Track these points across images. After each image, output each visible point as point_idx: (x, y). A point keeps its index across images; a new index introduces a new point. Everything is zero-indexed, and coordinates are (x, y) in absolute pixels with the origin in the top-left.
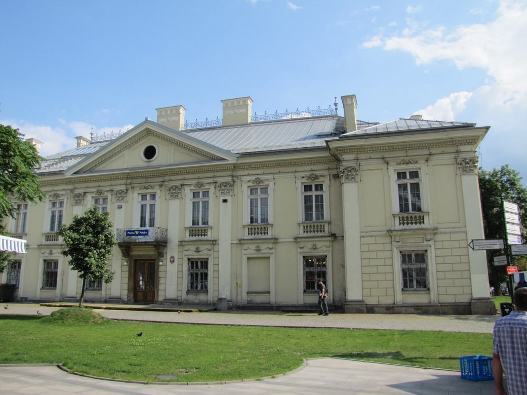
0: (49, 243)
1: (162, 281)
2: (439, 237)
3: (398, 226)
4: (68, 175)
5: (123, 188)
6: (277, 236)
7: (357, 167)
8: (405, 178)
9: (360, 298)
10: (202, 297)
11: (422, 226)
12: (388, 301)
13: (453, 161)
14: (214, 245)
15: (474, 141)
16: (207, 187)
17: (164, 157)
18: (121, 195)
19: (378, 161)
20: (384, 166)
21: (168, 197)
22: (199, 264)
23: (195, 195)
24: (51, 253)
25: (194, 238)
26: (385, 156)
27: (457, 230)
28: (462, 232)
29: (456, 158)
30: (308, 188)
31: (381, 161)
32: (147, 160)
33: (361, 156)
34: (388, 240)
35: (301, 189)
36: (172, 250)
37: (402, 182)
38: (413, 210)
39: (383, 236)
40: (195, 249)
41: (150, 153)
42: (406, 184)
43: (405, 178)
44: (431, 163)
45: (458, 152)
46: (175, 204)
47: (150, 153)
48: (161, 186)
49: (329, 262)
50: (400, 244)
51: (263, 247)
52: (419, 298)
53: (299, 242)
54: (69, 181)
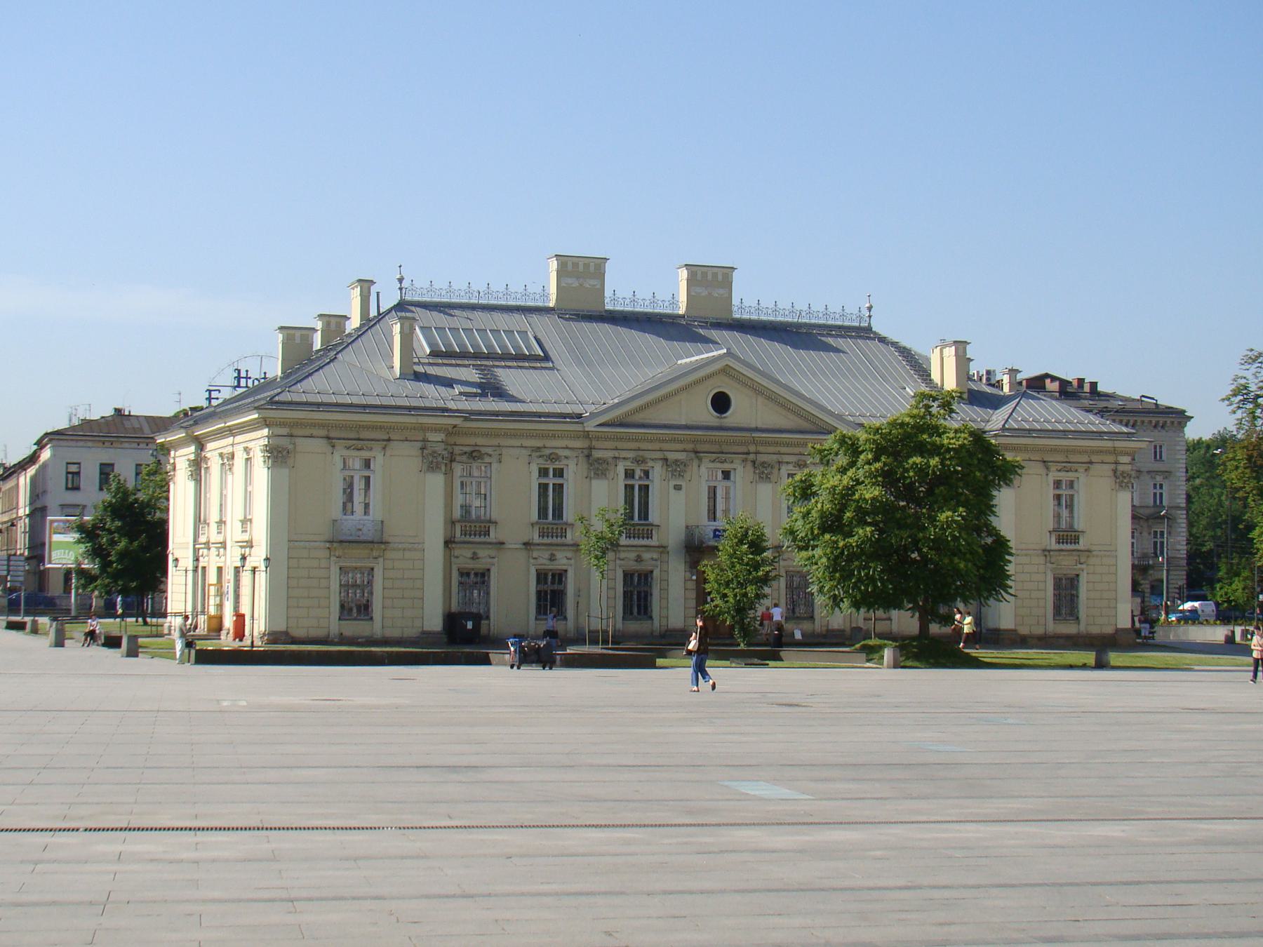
2: (1092, 561)
3: (1054, 546)
4: (590, 426)
5: (681, 456)
6: (501, 540)
9: (1011, 626)
12: (1039, 631)
13: (1111, 473)
16: (651, 464)
17: (743, 410)
18: (676, 468)
20: (1042, 470)
21: (425, 467)
23: (629, 474)
24: (552, 558)
25: (546, 540)
29: (1115, 471)
30: (543, 472)
34: (1042, 559)
35: (535, 473)
41: (721, 403)
46: (765, 490)
47: (721, 403)
52: (1069, 629)
54: (587, 435)
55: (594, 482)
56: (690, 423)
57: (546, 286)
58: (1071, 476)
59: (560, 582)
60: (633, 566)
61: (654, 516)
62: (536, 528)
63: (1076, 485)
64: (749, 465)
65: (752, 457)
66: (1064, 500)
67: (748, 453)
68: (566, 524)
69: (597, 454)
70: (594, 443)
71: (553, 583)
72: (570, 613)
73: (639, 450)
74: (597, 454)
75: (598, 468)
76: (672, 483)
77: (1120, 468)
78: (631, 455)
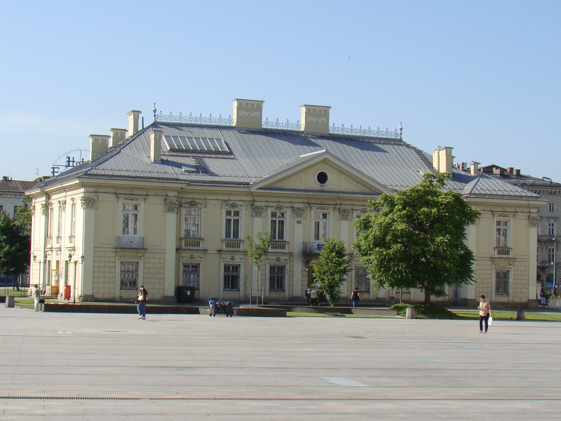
0: (229, 249)
2: (516, 264)
4: (253, 189)
5: (301, 206)
7: (96, 198)
11: (508, 256)
13: (527, 218)
14: (290, 256)
16: (285, 209)
21: (166, 210)
23: (274, 215)
24: (233, 258)
25: (229, 249)
29: (529, 217)
30: (228, 213)
31: (490, 213)
34: (490, 263)
35: (224, 214)
40: (230, 258)
41: (322, 178)
44: (517, 217)
46: (345, 224)
47: (322, 178)
49: (242, 267)
51: (236, 257)
54: (251, 194)
55: (256, 219)
58: (506, 219)
59: (237, 271)
60: (275, 263)
64: (337, 210)
65: (338, 206)
68: (285, 242)
70: (256, 198)
71: (233, 271)
72: (286, 288)
74: (257, 204)
75: (257, 211)
76: (296, 220)
78: (275, 204)
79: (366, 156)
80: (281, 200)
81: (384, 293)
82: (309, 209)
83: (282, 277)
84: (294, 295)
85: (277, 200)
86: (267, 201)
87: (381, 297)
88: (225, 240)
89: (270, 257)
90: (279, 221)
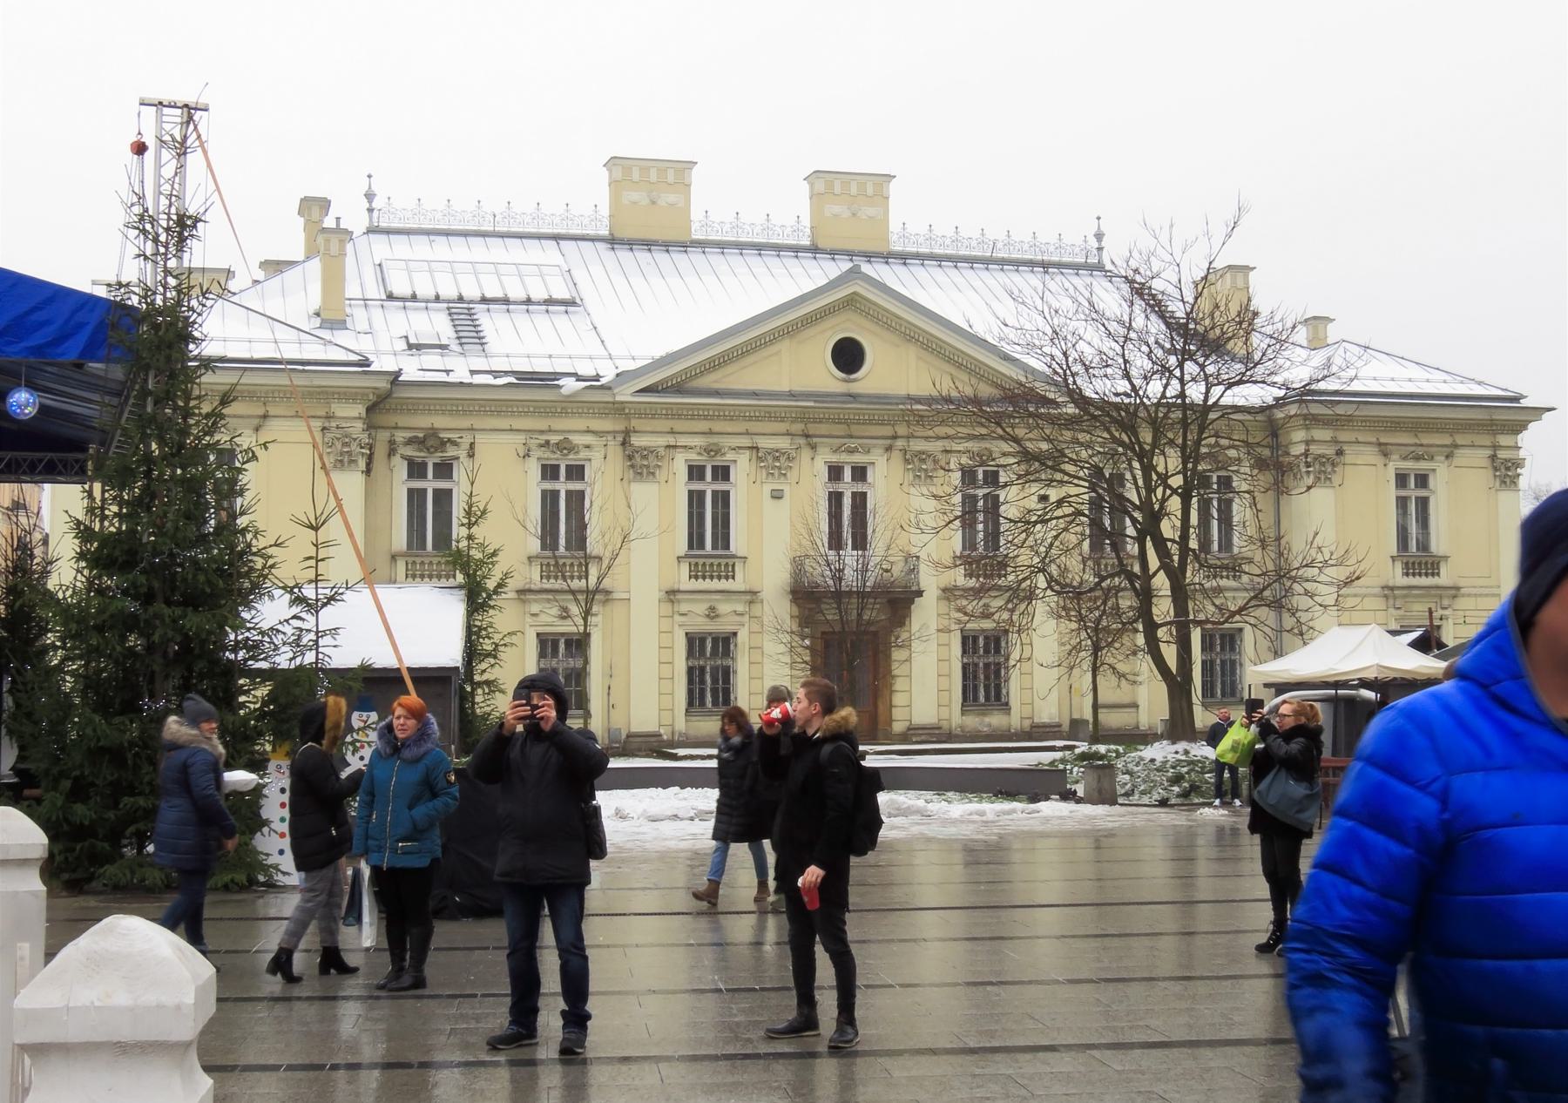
0: (547, 585)
1: (899, 684)
2: (1462, 603)
4: (625, 394)
5: (783, 443)
8: (702, 478)
10: (996, 720)
13: (1486, 463)
15: (1518, 427)
17: (891, 371)
19: (1369, 448)
20: (1379, 460)
22: (562, 646)
23: (695, 472)
26: (1341, 438)
27: (1486, 591)
28: (1493, 595)
29: (1493, 457)
30: (550, 472)
32: (844, 375)
33: (1344, 436)
36: (927, 615)
37: (697, 486)
38: (435, 547)
39: (1375, 596)
41: (848, 356)
42: (425, 490)
43: (702, 478)
44: (1457, 461)
45: (1495, 447)
46: (643, 492)
47: (848, 356)
48: (889, 449)
50: (1401, 612)
53: (529, 601)
54: (618, 409)
56: (797, 388)
57: (591, 204)
58: (1423, 465)
59: (727, 653)
60: (701, 625)
61: (738, 543)
62: (685, 568)
63: (1431, 482)
64: (897, 455)
65: (900, 443)
66: (1414, 509)
67: (895, 437)
68: (734, 557)
69: (637, 441)
70: (635, 423)
71: (987, 651)
72: (1014, 702)
73: (711, 433)
74: (637, 441)
75: (640, 464)
77: (1314, 449)
78: (698, 441)
79: (977, 283)
80: (718, 426)
81: (1054, 710)
82: (806, 454)
83: (1233, 663)
84: (635, 729)
85: (703, 426)
86: (672, 432)
87: (1046, 720)
88: (686, 556)
89: (684, 608)
90: (715, 493)
